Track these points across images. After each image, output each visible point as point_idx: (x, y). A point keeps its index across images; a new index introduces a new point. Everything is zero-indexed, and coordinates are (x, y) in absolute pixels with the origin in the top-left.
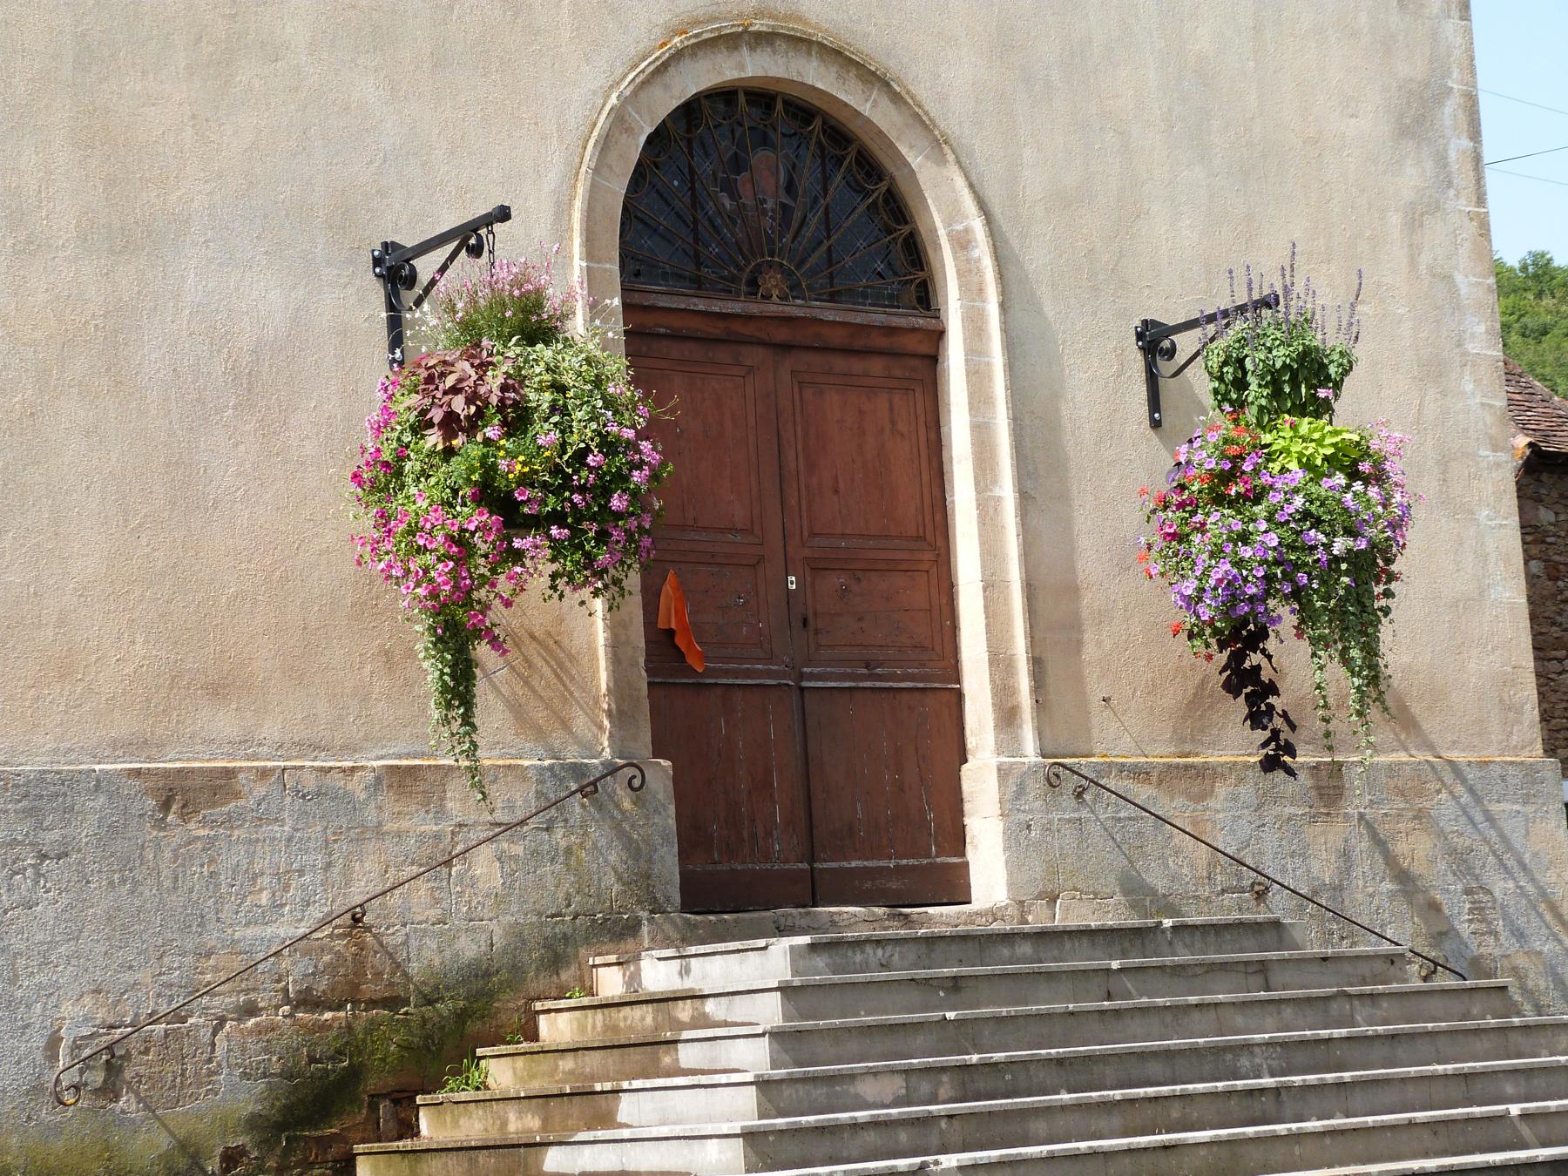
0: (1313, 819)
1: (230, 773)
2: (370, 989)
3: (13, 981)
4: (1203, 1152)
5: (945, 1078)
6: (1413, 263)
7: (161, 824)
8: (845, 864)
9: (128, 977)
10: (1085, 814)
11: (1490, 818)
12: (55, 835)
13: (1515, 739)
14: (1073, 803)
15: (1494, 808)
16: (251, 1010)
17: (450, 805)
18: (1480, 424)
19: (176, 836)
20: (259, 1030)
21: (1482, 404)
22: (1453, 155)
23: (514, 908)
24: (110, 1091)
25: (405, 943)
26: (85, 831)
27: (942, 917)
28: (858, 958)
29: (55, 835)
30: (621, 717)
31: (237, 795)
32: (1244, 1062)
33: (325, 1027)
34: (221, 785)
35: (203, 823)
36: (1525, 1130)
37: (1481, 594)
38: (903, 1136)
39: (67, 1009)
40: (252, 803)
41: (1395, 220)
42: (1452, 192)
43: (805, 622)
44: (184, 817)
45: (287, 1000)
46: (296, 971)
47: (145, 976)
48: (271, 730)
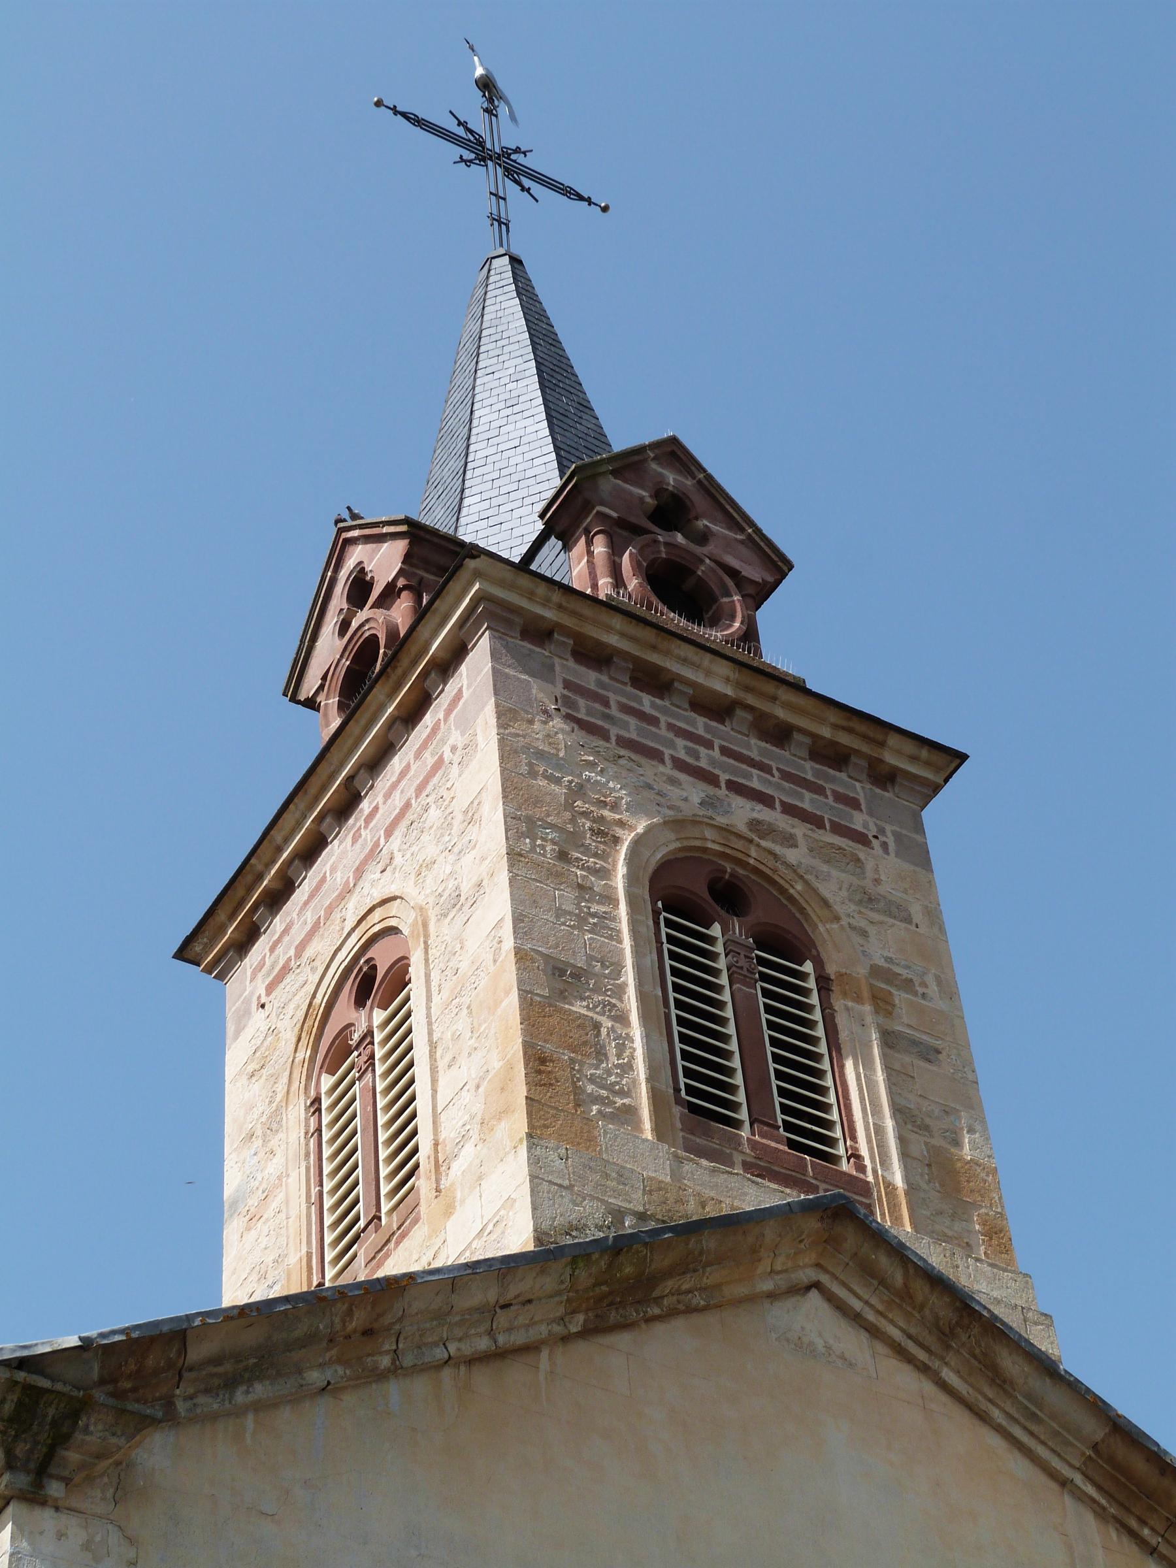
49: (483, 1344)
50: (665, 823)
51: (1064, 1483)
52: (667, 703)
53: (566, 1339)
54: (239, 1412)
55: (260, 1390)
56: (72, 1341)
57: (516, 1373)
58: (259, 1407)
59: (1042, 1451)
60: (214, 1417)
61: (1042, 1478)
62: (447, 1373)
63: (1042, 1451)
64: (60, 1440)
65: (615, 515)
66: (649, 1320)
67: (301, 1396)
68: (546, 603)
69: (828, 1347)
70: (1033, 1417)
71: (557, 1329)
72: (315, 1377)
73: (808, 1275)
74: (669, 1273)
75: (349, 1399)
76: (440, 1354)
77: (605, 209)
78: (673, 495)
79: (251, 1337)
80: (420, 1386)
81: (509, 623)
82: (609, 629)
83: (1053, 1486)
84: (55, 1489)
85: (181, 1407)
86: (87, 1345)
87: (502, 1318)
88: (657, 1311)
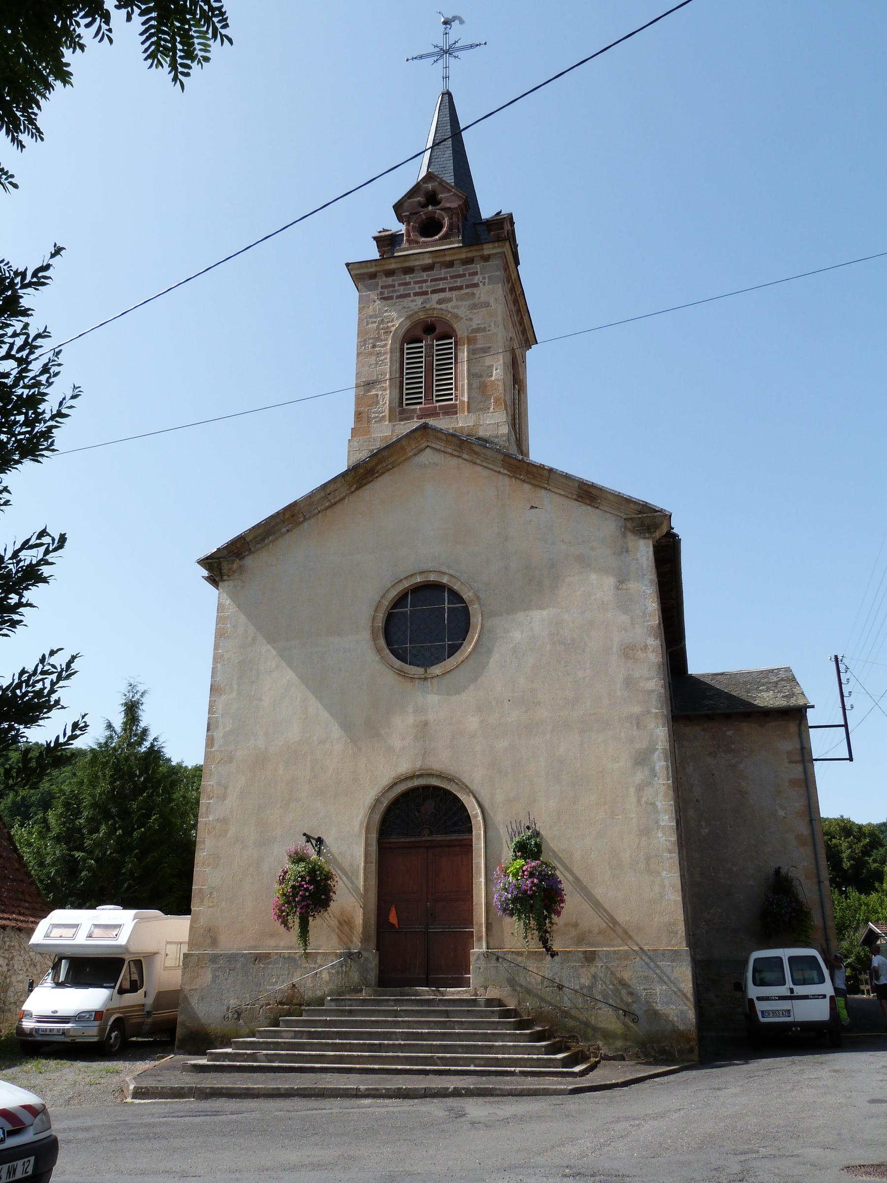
0: (582, 967)
1: (270, 953)
2: (295, 1001)
3: (222, 995)
4: (332, 1057)
5: (305, 1034)
6: (639, 801)
7: (254, 964)
8: (438, 976)
9: (244, 996)
10: (499, 965)
11: (658, 967)
12: (233, 966)
13: (673, 942)
14: (496, 962)
15: (659, 963)
16: (269, 1004)
17: (318, 961)
18: (665, 846)
19: (257, 966)
20: (270, 1008)
21: (666, 840)
22: (657, 767)
23: (331, 985)
24: (238, 1019)
25: (304, 992)
26: (239, 965)
27: (453, 993)
28: (343, 1003)
29: (233, 966)
30: (365, 939)
31: (271, 958)
32: (394, 1037)
33: (284, 1009)
34: (267, 956)
35: (263, 964)
36: (438, 1061)
37: (661, 897)
38: (272, 1046)
39: (232, 1001)
40: (273, 960)
41: (632, 790)
42: (656, 779)
43: (432, 915)
44: (259, 962)
45: (276, 1003)
46: (279, 997)
47: (247, 996)
48: (282, 944)
49: (327, 504)
50: (406, 318)
51: (499, 472)
52: (415, 275)
53: (352, 493)
54: (268, 544)
55: (271, 538)
56: (216, 550)
57: (339, 507)
58: (272, 541)
59: (491, 466)
60: (262, 548)
61: (493, 473)
62: (320, 515)
63: (491, 466)
64: (221, 569)
65: (408, 213)
66: (377, 477)
67: (282, 535)
68: (372, 267)
69: (430, 463)
70: (486, 459)
71: (348, 492)
72: (284, 530)
73: (426, 444)
74: (377, 465)
75: (295, 531)
76: (316, 511)
77: (485, 44)
78: (432, 191)
79: (261, 530)
80: (313, 521)
81: (364, 278)
82: (391, 263)
83: (497, 474)
84: (225, 578)
85: (253, 549)
86: (219, 549)
87: (330, 497)
88: (377, 475)
